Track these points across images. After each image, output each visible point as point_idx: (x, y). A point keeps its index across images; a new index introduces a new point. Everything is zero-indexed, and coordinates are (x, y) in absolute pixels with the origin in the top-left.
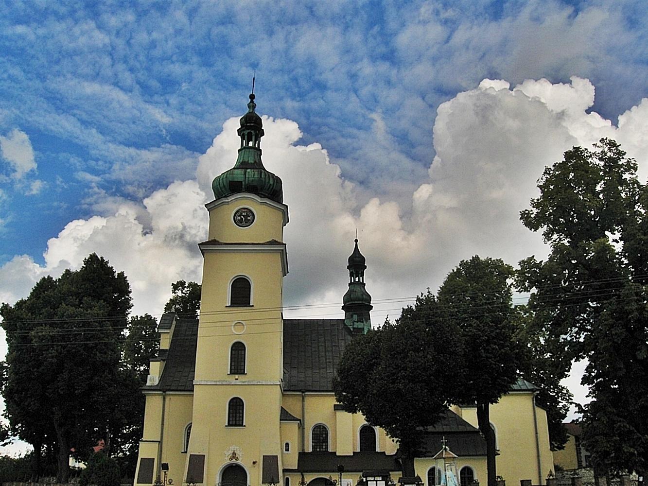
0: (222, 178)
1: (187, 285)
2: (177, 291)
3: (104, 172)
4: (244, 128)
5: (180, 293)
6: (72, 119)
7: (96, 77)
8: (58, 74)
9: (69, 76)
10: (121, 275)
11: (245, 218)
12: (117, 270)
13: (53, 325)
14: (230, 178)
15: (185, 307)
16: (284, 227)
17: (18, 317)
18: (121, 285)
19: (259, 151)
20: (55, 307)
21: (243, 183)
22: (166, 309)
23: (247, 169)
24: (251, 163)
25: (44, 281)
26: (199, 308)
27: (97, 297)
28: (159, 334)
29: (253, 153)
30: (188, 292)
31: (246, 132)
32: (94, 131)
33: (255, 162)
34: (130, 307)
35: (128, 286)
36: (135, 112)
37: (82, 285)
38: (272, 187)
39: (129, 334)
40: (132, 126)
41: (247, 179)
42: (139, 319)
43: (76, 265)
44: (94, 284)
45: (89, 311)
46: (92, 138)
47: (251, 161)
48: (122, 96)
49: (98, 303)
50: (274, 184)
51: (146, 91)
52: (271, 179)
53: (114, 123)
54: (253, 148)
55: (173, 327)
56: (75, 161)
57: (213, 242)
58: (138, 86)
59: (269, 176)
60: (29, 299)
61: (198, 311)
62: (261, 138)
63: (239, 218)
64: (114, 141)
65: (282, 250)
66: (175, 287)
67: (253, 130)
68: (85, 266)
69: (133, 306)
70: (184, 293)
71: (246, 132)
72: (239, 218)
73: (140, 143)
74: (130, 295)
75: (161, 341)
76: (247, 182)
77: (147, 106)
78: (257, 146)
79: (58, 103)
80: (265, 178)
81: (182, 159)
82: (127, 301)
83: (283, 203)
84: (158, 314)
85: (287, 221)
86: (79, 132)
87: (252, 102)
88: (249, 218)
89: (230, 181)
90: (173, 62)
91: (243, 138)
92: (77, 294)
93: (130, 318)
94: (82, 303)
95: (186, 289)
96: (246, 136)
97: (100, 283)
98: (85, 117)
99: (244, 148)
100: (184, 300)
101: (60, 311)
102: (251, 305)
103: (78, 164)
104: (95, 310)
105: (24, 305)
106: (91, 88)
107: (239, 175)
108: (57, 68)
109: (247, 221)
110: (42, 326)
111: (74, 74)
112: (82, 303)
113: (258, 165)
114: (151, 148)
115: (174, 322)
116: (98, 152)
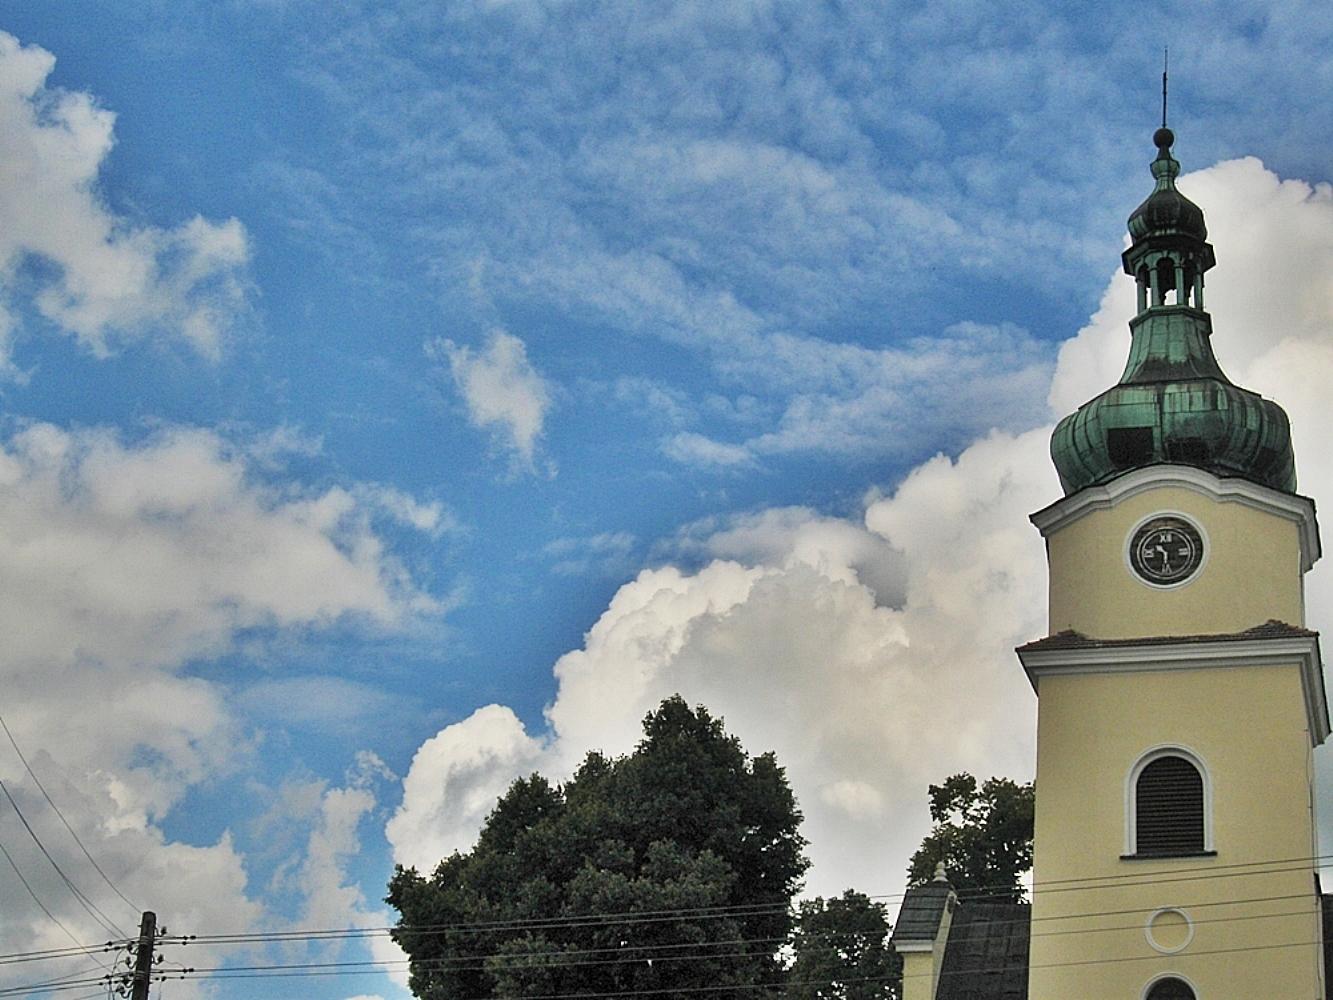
0: (1080, 421)
1: (979, 790)
2: (948, 811)
3: (757, 430)
4: (1145, 246)
5: (956, 819)
6: (657, 266)
7: (728, 124)
8: (615, 127)
9: (646, 130)
10: (766, 764)
11: (1168, 553)
12: (752, 749)
13: (558, 936)
14: (1111, 420)
15: (976, 865)
16: (1306, 575)
17: (448, 911)
18: (766, 800)
19: (1201, 321)
20: (560, 876)
21: (1156, 432)
22: (915, 874)
23: (1166, 383)
24: (1178, 364)
25: (520, 793)
26: (1026, 865)
27: (692, 838)
28: (898, 961)
29: (1181, 329)
30: (986, 815)
31: (1152, 260)
32: (727, 299)
33: (1191, 357)
34: (799, 870)
35: (787, 798)
36: (860, 226)
37: (644, 800)
38: (1255, 437)
39: (794, 959)
40: (849, 273)
41: (1167, 417)
42: (826, 908)
43: (622, 741)
44: (679, 796)
45: (670, 887)
46: (720, 321)
47: (1177, 356)
48: (814, 177)
49: (696, 858)
50: (1261, 425)
51: (891, 154)
52: (1251, 411)
53: (787, 269)
54: (1182, 310)
55: (943, 934)
56: (662, 398)
57: (1064, 641)
58: (868, 142)
59: (1243, 405)
60: (479, 852)
61: (1025, 879)
62: (1205, 274)
63: (1150, 553)
64: (792, 327)
65: (1306, 655)
66: (941, 799)
67: (1174, 251)
68: (648, 739)
69: (808, 864)
70: (973, 818)
71: (1152, 260)
72: (1150, 553)
73: (872, 328)
74: (800, 829)
75: (906, 983)
76: (1167, 428)
77: (896, 201)
78: (1192, 303)
79: (610, 219)
80: (1230, 410)
81: (1018, 369)
82: (790, 848)
83: (1297, 493)
84: (888, 889)
85: (1314, 552)
86: (680, 308)
87: (1165, 155)
88: (1183, 552)
89: (1110, 431)
90: (978, 49)
91: (1144, 281)
92: (628, 834)
93: (796, 907)
94: (647, 860)
95: (976, 804)
96: (1153, 275)
97: (702, 796)
98: (694, 253)
99: (1151, 314)
100: (970, 842)
101: (577, 885)
102: (1208, 848)
103: (673, 410)
104: (690, 884)
105: (462, 873)
106: (715, 161)
107: (1140, 408)
108: (604, 110)
109: (1177, 562)
110: (524, 937)
111: (662, 122)
112: (647, 860)
113: (1204, 369)
114: (914, 341)
115: (947, 918)
116: (738, 364)
